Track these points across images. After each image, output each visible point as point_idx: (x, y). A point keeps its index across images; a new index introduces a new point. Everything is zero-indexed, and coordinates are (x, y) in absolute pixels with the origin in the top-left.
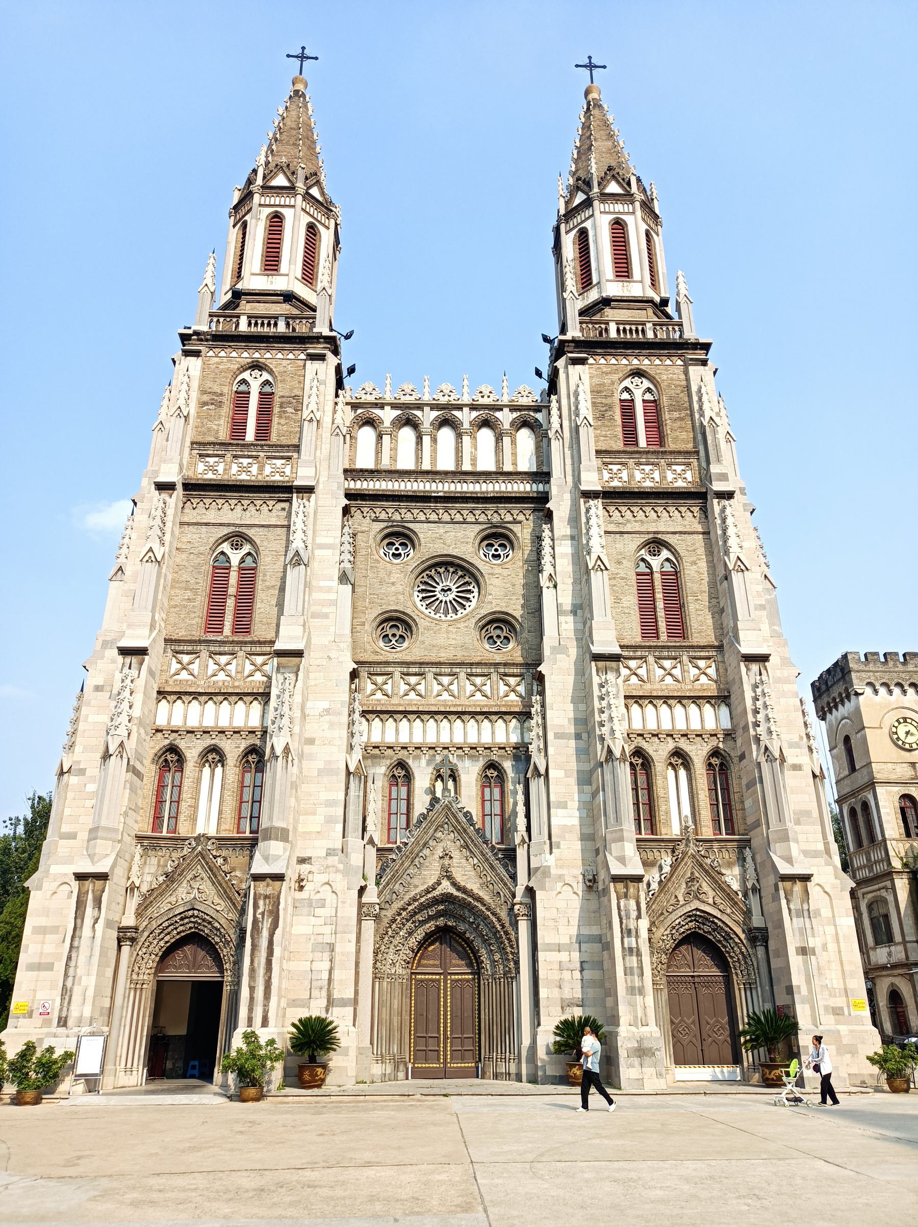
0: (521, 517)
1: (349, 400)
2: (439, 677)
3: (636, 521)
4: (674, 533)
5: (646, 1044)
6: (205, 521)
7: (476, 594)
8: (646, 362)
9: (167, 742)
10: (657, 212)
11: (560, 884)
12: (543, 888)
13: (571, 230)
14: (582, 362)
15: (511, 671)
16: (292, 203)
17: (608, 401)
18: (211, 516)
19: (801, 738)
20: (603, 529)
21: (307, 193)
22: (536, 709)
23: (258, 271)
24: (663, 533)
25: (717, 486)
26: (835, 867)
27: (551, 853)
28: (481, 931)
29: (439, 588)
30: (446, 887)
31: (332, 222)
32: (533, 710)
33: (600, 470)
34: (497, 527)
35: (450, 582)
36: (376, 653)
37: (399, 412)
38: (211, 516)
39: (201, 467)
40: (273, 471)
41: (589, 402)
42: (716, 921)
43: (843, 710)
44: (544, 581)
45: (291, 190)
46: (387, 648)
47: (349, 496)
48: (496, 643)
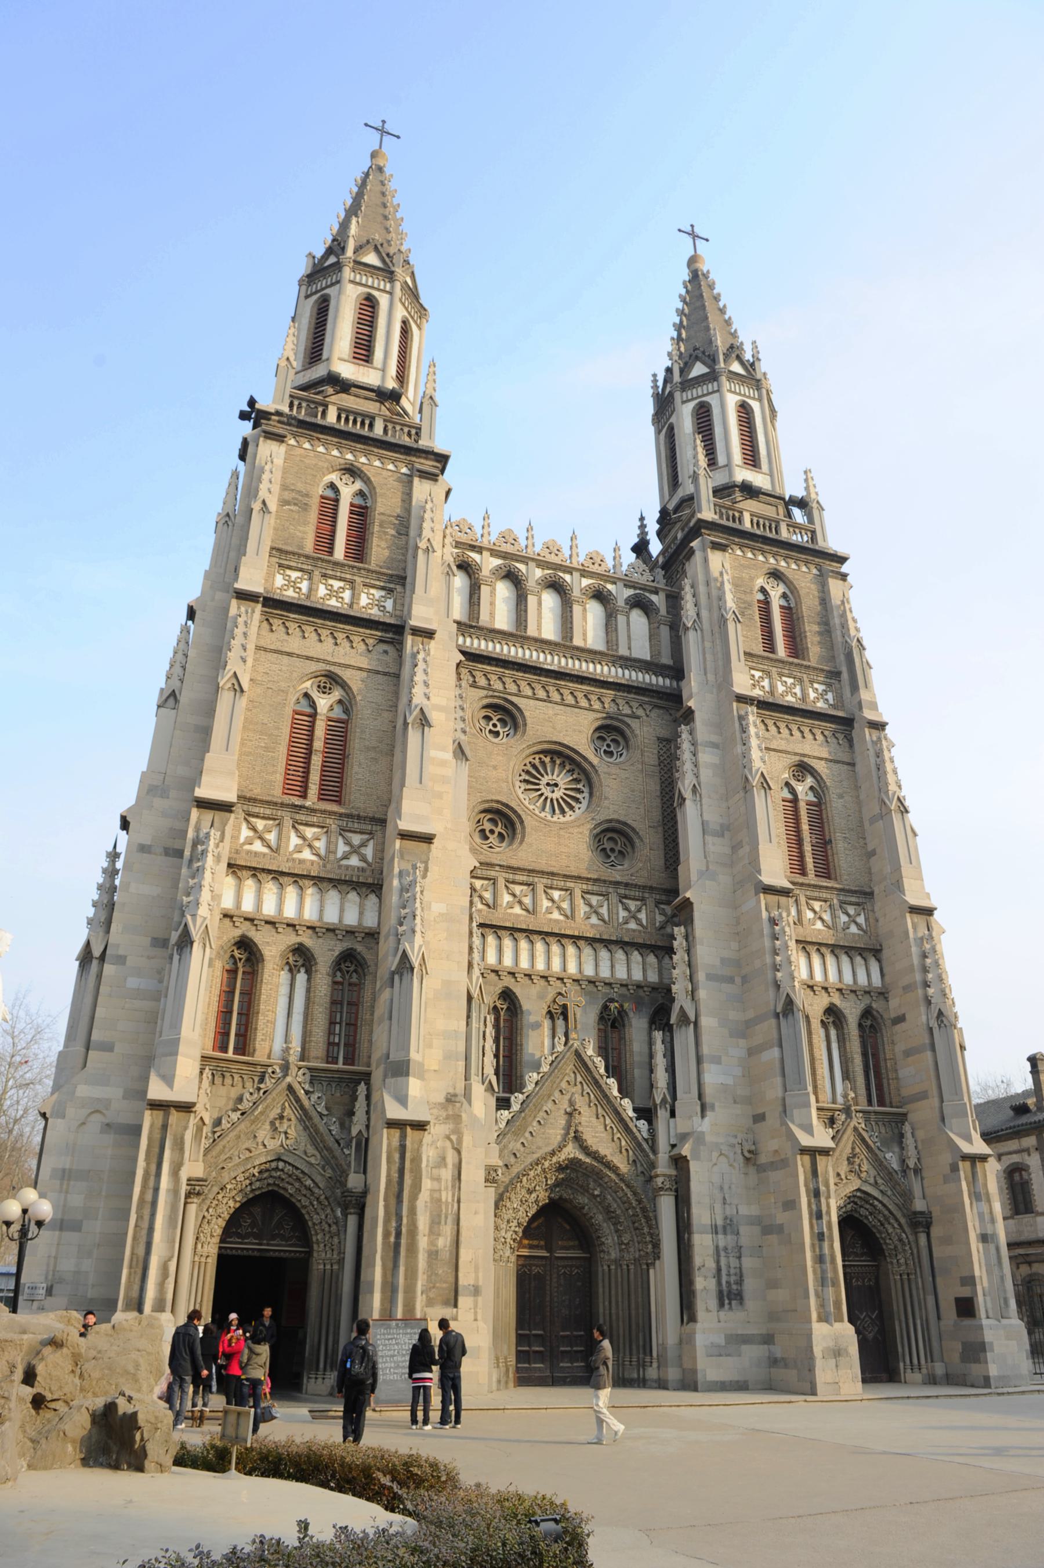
0: (640, 712)
2: (549, 891)
6: (287, 650)
7: (586, 795)
11: (715, 1154)
12: (697, 1158)
13: (688, 401)
15: (632, 893)
18: (294, 643)
22: (679, 943)
23: (346, 357)
27: (703, 1117)
28: (609, 1206)
30: (571, 1151)
32: (676, 944)
35: (563, 779)
39: (279, 581)
42: (876, 1203)
48: (609, 857)
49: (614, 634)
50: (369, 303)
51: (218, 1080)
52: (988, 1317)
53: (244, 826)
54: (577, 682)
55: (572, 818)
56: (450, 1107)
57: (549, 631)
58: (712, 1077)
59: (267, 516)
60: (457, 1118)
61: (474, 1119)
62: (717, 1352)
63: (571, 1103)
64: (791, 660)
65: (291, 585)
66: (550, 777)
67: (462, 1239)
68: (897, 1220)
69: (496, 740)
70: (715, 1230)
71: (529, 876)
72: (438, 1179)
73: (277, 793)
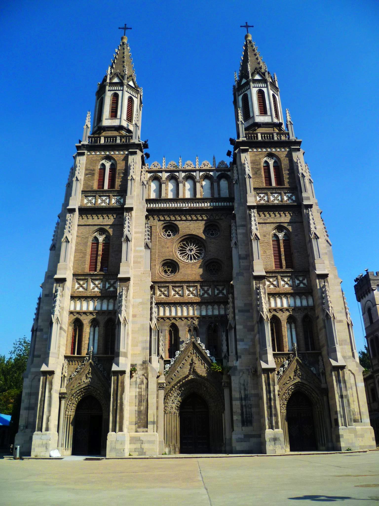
1: (147, 169)
5: (277, 436)
6: (88, 224)
7: (204, 251)
8: (274, 150)
9: (75, 317)
10: (277, 86)
12: (234, 375)
13: (240, 94)
14: (246, 151)
17: (258, 167)
18: (90, 221)
19: (343, 309)
20: (257, 221)
21: (128, 84)
22: (230, 300)
23: (108, 118)
25: (305, 202)
26: (356, 362)
29: (188, 249)
31: (139, 95)
33: (255, 197)
36: (161, 278)
37: (169, 174)
38: (90, 221)
39: (85, 201)
42: (307, 386)
43: (367, 298)
44: (232, 245)
45: (121, 84)
46: (166, 276)
47: (148, 210)
50: (116, 96)
51: (71, 363)
52: (342, 426)
53: (76, 284)
56: (144, 365)
57: (188, 195)
58: (240, 346)
59: (78, 182)
60: (146, 369)
61: (152, 368)
62: (240, 440)
63: (192, 360)
64: (279, 187)
65: (88, 202)
67: (149, 406)
68: (315, 392)
69: (170, 238)
70: (241, 399)
71: (179, 284)
72: (141, 388)
73: (87, 270)
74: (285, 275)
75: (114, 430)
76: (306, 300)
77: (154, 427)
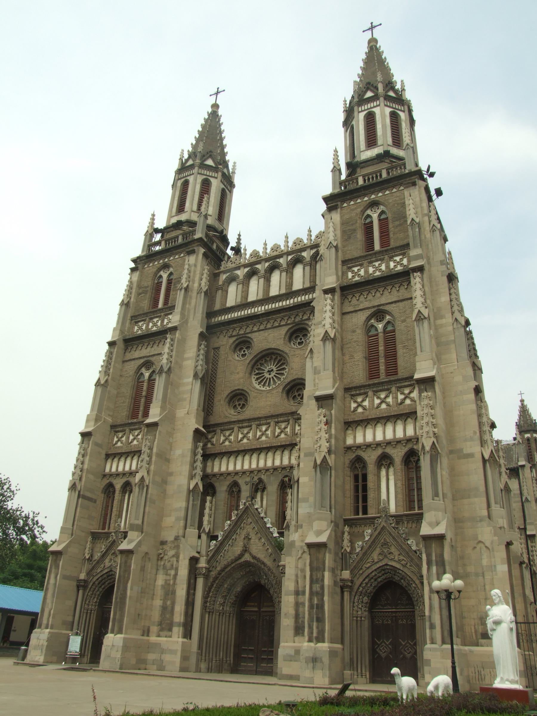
3: (366, 301)
4: (392, 303)
6: (133, 358)
9: (108, 481)
16: (216, 176)
19: (475, 433)
24: (383, 305)
29: (266, 370)
30: (247, 557)
34: (299, 324)
39: (371, 270)
40: (396, 264)
41: (407, 209)
42: (401, 572)
49: (312, 274)
54: (277, 314)
55: (260, 388)
66: (268, 368)
74: (380, 388)
75: (112, 632)
76: (412, 425)
77: (179, 632)
